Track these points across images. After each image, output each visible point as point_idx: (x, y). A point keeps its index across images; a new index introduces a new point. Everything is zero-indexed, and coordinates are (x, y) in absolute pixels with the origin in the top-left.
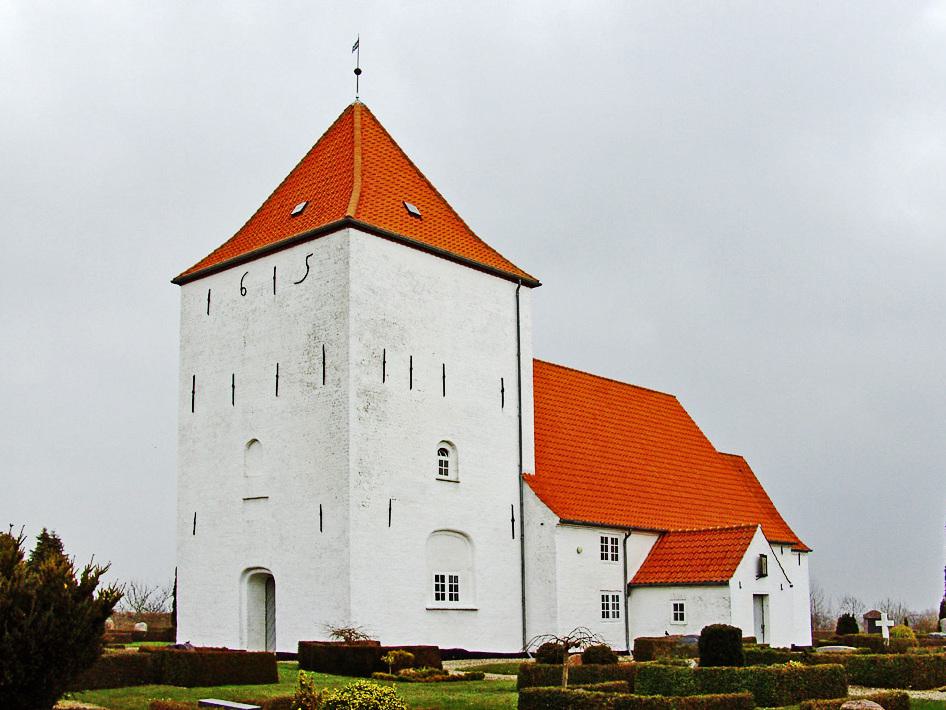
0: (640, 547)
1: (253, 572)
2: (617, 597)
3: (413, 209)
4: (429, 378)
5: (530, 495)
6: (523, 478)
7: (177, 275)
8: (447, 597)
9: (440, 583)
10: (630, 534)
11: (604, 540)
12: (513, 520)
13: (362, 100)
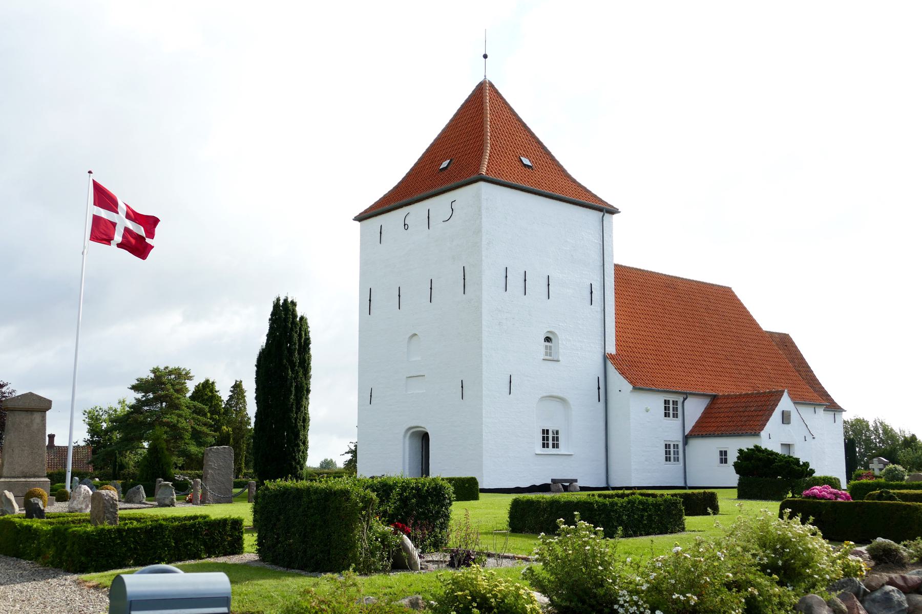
0: (694, 409)
2: (677, 445)
3: (526, 161)
4: (537, 286)
5: (611, 368)
6: (606, 357)
7: (357, 214)
8: (551, 445)
9: (545, 435)
11: (667, 402)
12: (599, 388)
13: (489, 78)
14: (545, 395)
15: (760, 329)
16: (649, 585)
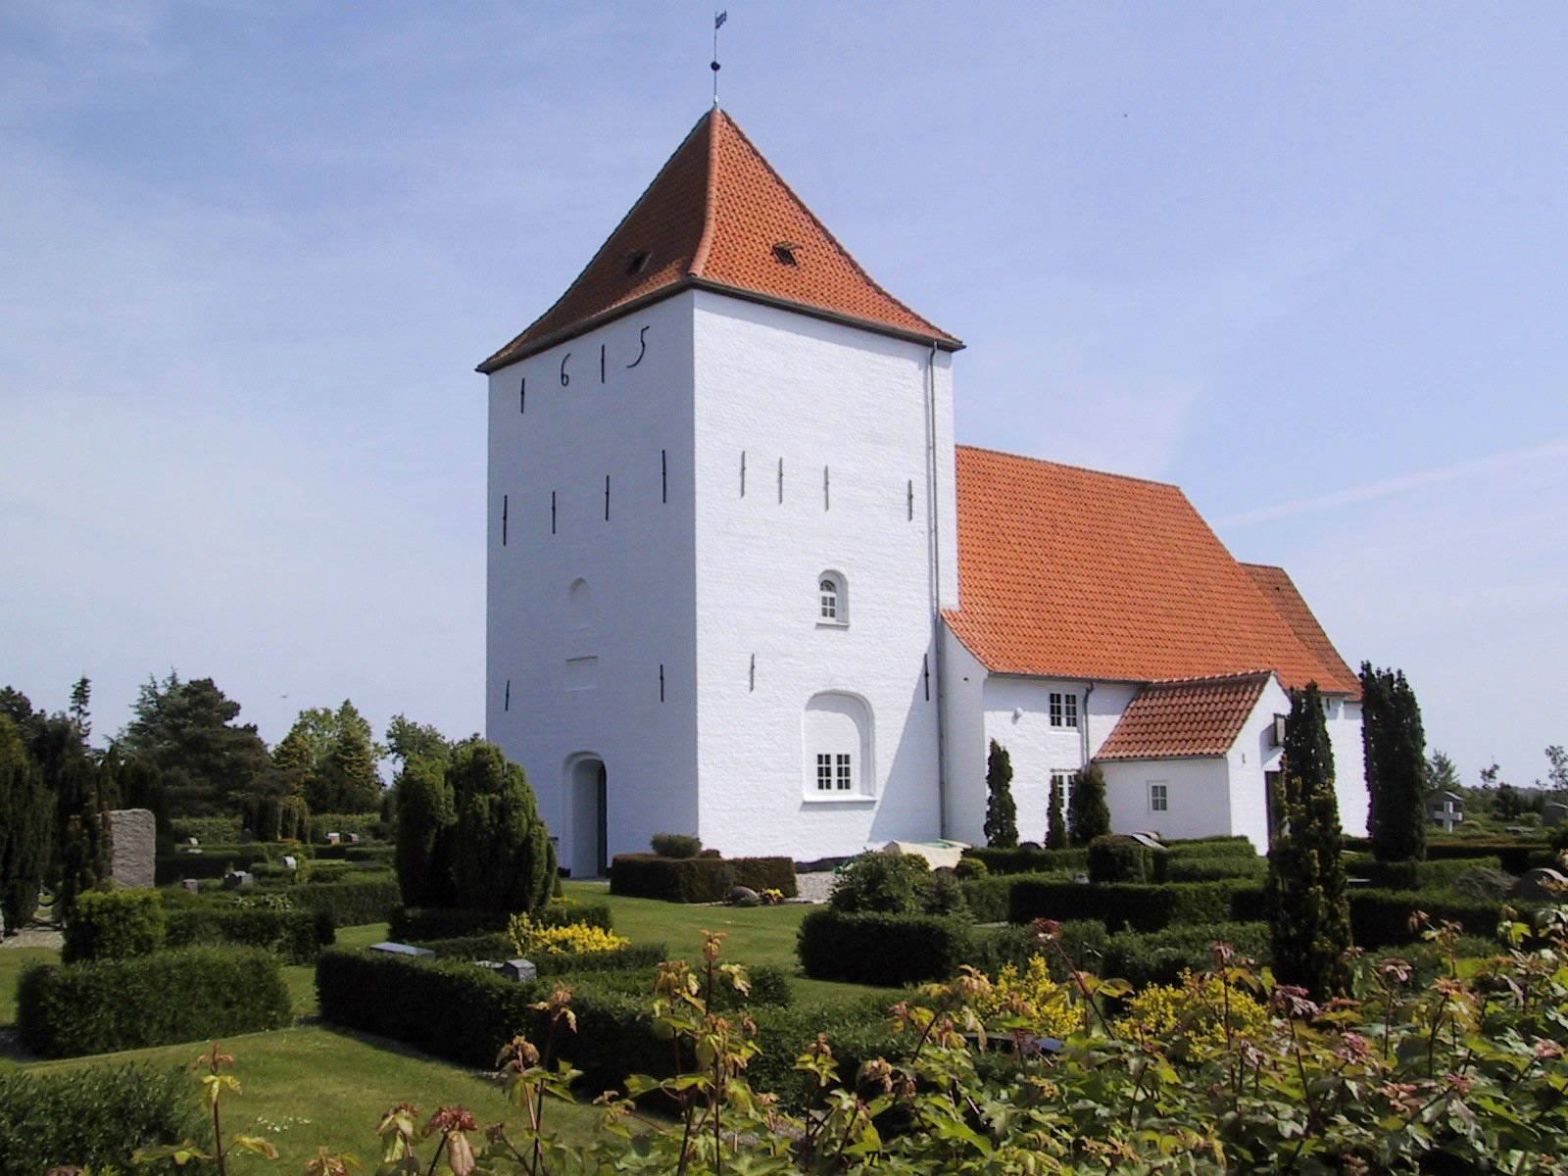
1: (581, 758)
10: (1092, 689)
14: (821, 689)
15: (1230, 559)
16: (251, 783)
